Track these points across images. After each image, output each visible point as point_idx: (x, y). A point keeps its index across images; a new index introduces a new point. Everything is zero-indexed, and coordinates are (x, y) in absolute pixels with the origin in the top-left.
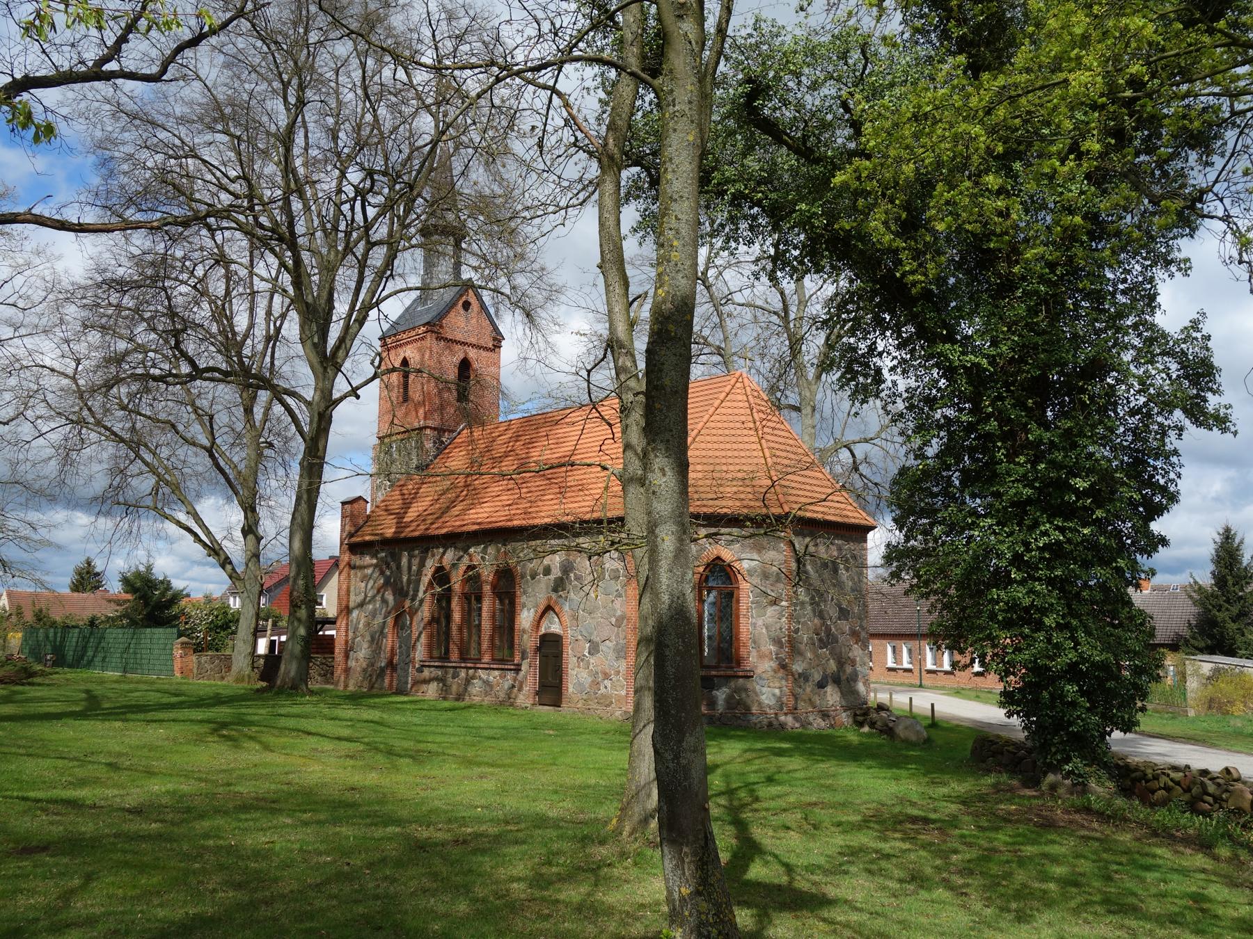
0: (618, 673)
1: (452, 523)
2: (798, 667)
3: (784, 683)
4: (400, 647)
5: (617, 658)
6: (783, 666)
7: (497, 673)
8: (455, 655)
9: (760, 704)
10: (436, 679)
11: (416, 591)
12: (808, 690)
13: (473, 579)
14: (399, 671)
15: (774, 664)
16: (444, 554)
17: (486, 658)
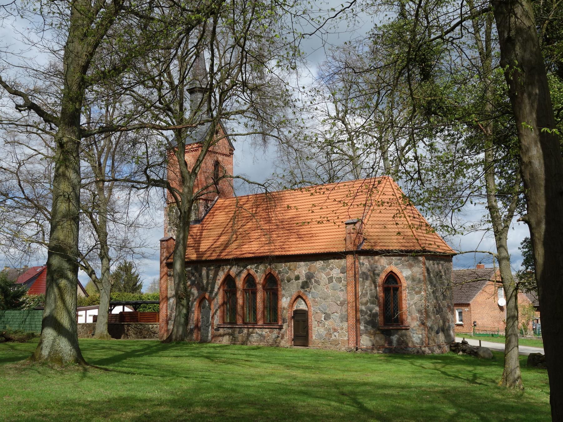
0: (342, 329)
1: (233, 252)
2: (429, 324)
3: (423, 331)
4: (202, 318)
5: (342, 322)
6: (423, 324)
7: (267, 330)
8: (240, 321)
9: (413, 342)
10: (228, 334)
11: (213, 288)
12: (433, 335)
13: (250, 280)
14: (202, 330)
15: (418, 323)
16: (230, 269)
17: (260, 323)
